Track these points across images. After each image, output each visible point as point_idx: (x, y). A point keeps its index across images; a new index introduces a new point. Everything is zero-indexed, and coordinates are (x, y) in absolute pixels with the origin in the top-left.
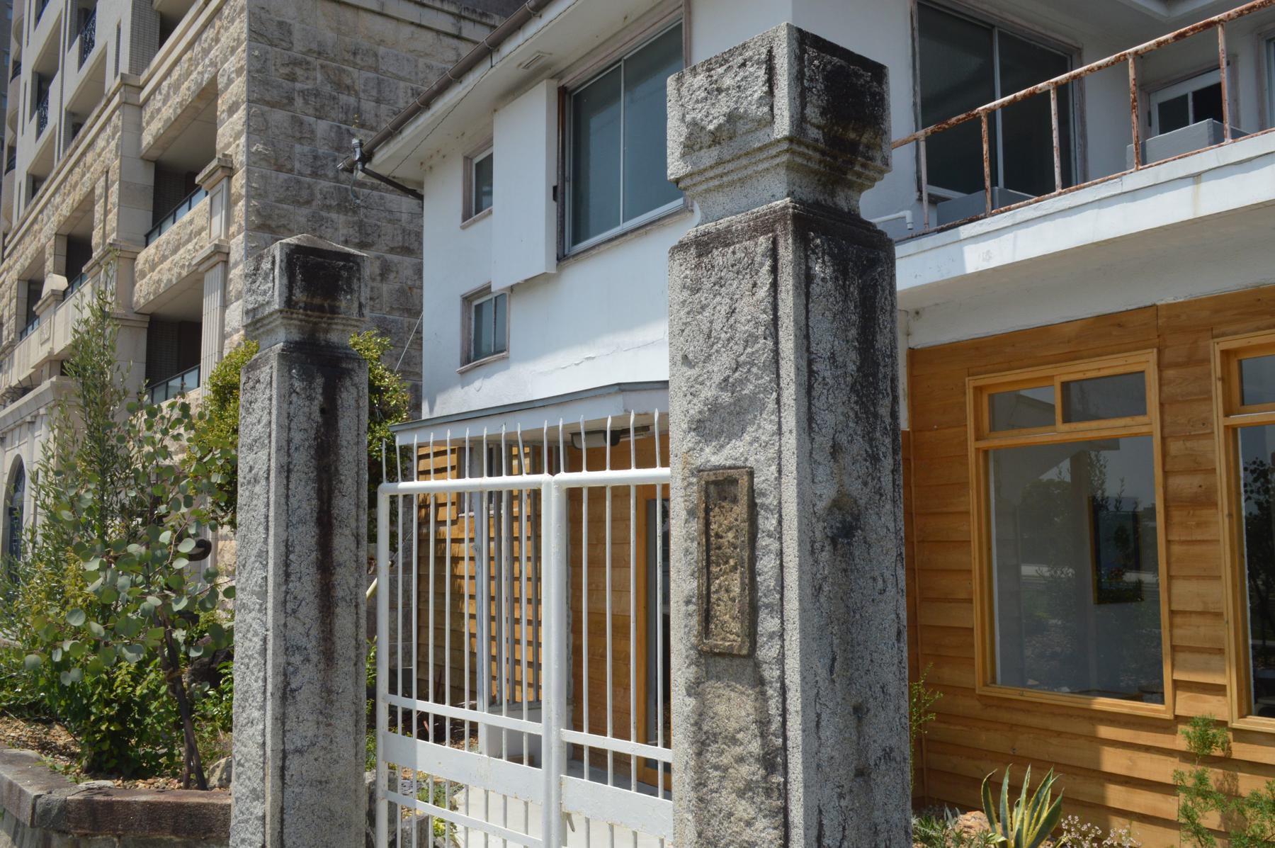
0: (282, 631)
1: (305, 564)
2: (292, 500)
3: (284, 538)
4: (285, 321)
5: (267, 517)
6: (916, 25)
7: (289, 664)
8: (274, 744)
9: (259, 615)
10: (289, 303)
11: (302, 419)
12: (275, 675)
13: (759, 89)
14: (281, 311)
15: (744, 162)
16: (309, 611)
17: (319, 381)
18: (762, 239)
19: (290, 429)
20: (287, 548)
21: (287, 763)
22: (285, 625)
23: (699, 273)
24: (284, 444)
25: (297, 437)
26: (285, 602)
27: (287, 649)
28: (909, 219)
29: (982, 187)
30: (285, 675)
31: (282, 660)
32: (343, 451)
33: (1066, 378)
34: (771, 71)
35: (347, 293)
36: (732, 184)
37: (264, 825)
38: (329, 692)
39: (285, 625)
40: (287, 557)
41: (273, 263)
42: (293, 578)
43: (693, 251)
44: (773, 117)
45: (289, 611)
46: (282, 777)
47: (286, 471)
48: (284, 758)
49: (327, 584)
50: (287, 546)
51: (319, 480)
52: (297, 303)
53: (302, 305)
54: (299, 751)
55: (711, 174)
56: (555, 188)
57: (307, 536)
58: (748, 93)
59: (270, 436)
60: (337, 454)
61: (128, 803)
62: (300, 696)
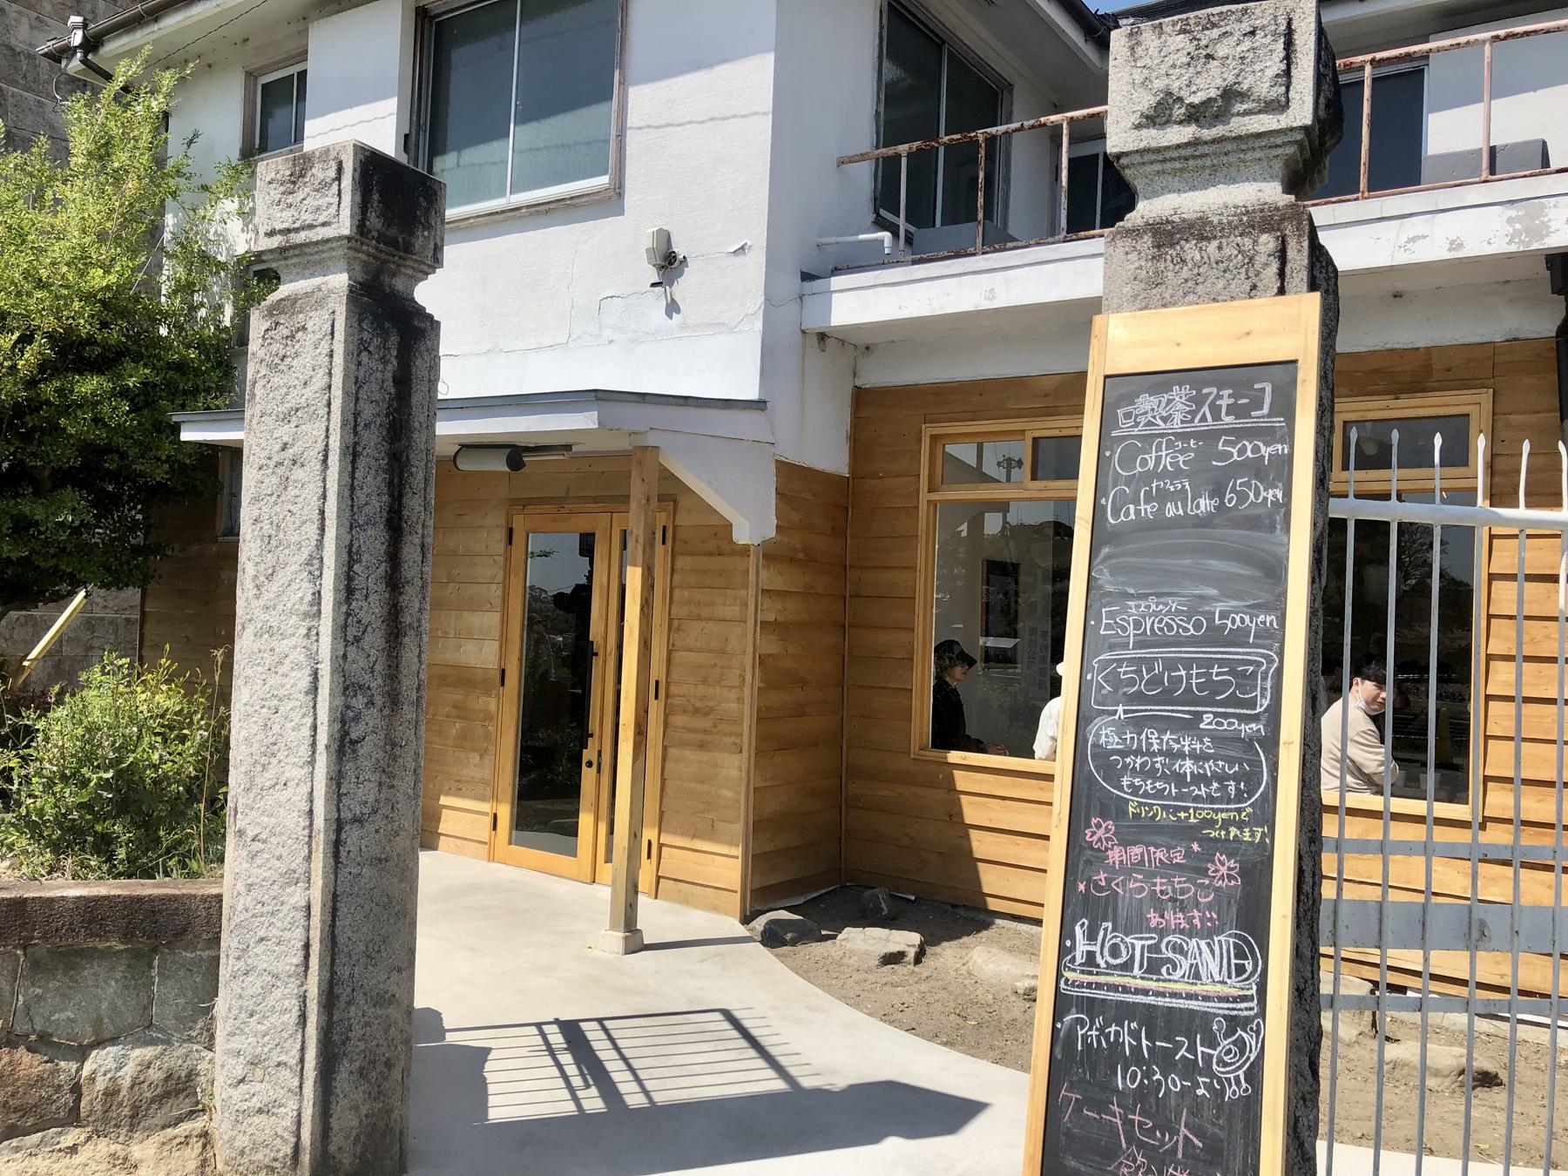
0: (341, 663)
1: (371, 575)
2: (358, 493)
3: (347, 542)
4: (352, 253)
5: (322, 512)
6: (885, 22)
7: (348, 707)
8: (327, 812)
9: (305, 642)
10: (361, 227)
11: (375, 387)
12: (332, 722)
13: (1275, 65)
14: (349, 238)
15: (1229, 147)
16: (375, 640)
17: (394, 339)
18: (1264, 238)
19: (357, 399)
20: (350, 557)
21: (344, 836)
22: (345, 656)
23: (1162, 266)
24: (351, 417)
25: (368, 411)
26: (345, 626)
27: (346, 688)
28: (886, 244)
29: (975, 219)
30: (343, 722)
31: (339, 701)
32: (416, 436)
33: (1037, 434)
34: (1289, 44)
35: (425, 228)
36: (1198, 169)
37: (308, 917)
38: (394, 745)
39: (345, 656)
40: (350, 568)
41: (340, 170)
42: (357, 595)
43: (1147, 239)
44: (1288, 100)
45: (350, 638)
46: (336, 855)
47: (352, 454)
48: (339, 830)
49: (395, 606)
50: (350, 553)
51: (390, 470)
52: (369, 231)
53: (375, 234)
54: (359, 821)
55: (1175, 154)
56: (407, 137)
57: (374, 541)
58: (1257, 67)
59: (329, 405)
60: (409, 439)
61: (52, 900)
62: (363, 750)
